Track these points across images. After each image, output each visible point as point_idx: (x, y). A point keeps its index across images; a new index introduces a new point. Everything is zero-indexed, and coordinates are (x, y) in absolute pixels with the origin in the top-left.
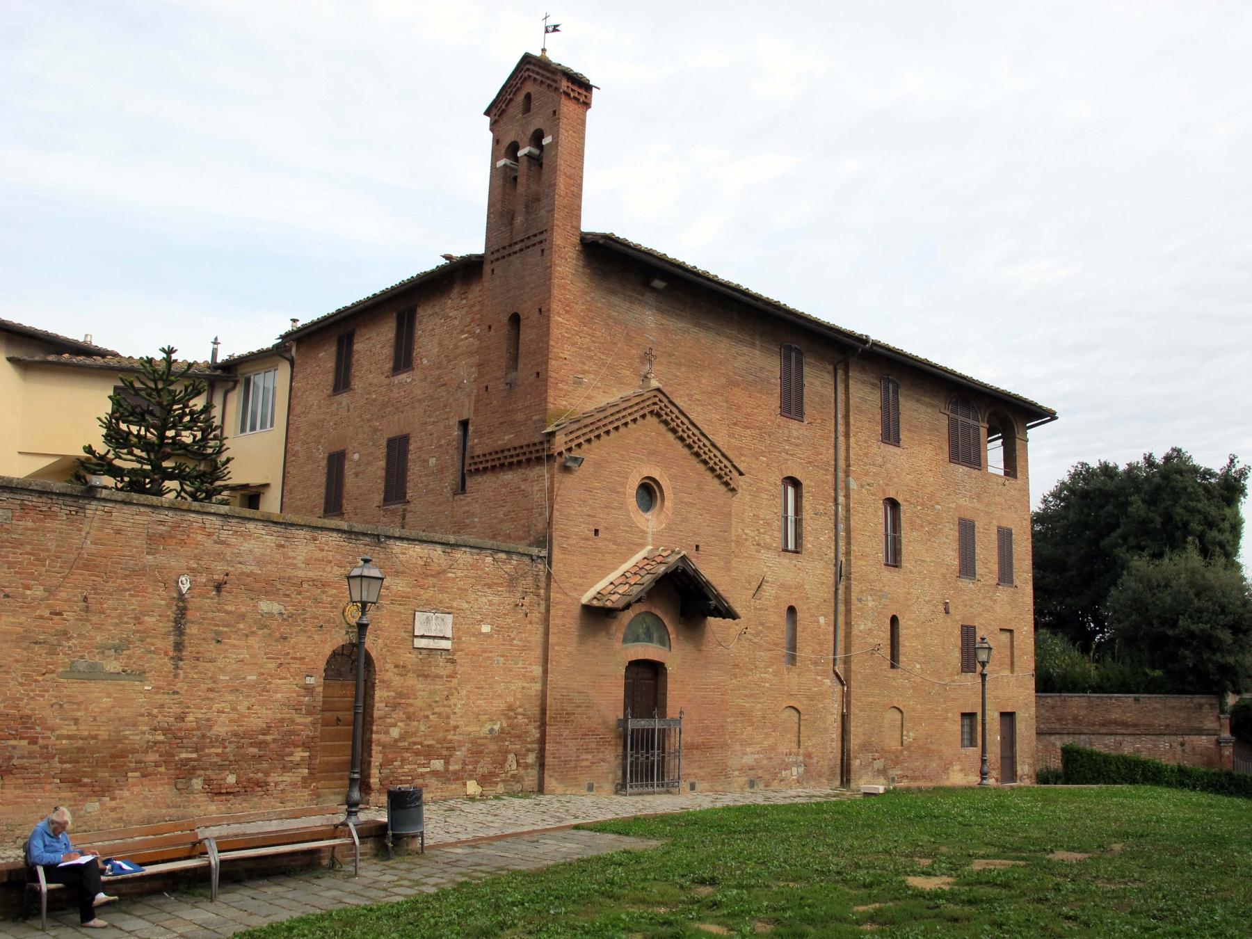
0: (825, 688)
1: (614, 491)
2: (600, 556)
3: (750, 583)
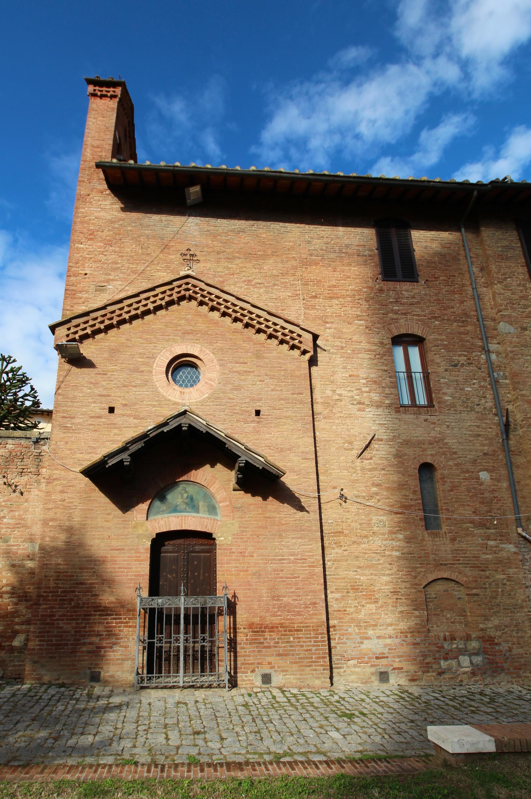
0: (504, 554)
1: (136, 370)
2: (116, 431)
3: (351, 443)
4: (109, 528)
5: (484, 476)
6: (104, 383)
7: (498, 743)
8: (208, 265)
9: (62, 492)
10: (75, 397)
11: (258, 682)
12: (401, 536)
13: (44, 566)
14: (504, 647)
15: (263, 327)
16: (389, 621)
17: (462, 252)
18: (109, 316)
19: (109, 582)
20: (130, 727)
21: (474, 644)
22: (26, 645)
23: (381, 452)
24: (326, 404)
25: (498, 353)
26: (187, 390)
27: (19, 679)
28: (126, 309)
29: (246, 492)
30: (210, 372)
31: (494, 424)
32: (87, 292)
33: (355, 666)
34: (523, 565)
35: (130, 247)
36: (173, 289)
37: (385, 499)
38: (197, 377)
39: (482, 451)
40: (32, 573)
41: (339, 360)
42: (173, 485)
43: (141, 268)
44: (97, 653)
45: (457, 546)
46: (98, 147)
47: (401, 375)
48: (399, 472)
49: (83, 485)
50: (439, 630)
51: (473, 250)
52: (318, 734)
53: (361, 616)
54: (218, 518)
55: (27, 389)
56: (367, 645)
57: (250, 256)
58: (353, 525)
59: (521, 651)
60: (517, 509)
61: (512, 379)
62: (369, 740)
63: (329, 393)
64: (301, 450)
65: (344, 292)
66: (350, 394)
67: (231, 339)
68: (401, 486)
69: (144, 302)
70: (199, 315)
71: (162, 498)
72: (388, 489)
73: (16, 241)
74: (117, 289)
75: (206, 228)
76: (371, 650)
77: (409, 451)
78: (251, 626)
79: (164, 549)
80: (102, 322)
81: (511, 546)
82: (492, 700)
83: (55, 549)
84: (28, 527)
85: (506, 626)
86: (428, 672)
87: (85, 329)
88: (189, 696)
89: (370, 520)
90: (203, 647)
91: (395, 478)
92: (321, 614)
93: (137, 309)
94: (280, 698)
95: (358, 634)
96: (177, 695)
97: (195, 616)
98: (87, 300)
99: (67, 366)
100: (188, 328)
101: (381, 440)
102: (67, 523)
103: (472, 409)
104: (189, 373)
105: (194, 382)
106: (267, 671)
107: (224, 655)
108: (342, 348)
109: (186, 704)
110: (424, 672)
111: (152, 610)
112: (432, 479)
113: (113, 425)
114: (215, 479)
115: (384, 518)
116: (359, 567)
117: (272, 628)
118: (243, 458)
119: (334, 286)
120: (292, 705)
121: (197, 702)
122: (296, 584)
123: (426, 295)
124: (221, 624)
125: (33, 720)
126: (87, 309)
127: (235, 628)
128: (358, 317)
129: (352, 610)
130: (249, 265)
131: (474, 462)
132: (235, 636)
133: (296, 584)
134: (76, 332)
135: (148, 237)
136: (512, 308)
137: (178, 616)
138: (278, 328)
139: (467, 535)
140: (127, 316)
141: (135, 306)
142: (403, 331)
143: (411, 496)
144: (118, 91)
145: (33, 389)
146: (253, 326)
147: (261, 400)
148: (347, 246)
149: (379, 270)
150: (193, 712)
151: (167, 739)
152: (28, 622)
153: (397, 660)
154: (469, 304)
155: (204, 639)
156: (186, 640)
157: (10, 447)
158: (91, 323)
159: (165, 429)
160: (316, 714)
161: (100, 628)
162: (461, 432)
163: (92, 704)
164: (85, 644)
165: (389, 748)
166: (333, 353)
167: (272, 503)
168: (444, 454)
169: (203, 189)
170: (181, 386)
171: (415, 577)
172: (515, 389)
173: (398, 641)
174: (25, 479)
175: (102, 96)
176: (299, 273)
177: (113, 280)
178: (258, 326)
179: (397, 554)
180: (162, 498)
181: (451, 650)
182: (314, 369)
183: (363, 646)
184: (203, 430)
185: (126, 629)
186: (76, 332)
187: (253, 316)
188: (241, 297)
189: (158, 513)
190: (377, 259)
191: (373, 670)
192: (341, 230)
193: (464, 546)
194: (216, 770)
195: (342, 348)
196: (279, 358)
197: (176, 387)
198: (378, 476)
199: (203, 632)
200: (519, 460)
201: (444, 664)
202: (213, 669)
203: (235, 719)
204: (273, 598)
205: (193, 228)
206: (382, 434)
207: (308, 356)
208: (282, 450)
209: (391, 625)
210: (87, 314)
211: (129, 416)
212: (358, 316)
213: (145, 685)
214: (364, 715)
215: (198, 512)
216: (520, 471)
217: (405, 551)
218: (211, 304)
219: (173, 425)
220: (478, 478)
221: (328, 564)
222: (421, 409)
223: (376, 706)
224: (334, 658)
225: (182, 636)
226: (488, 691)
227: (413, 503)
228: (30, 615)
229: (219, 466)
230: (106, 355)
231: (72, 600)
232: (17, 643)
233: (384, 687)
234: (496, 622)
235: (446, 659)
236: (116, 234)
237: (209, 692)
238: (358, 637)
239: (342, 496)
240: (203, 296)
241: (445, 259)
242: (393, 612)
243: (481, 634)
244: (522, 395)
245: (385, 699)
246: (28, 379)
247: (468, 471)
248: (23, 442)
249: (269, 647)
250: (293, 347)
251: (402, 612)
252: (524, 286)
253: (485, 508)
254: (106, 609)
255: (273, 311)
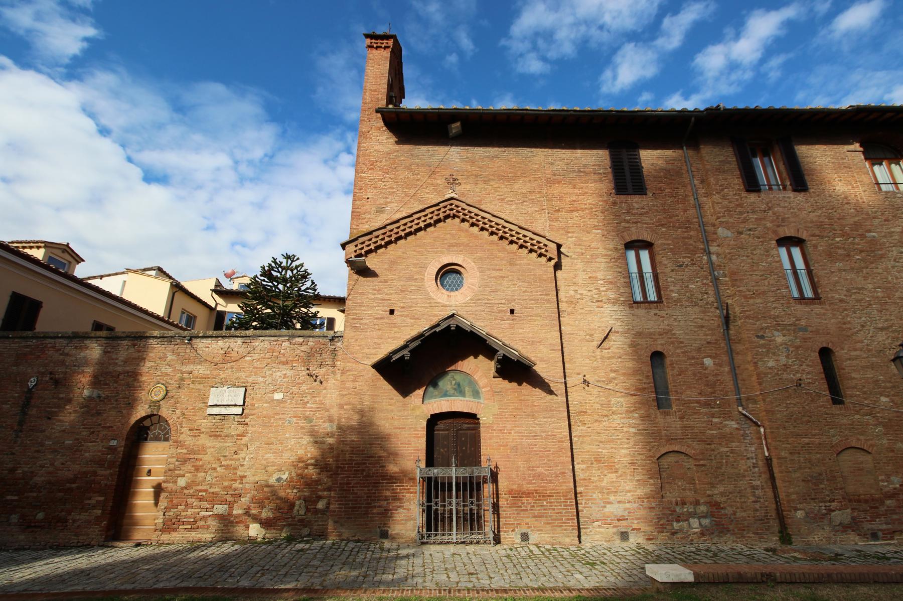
0: (727, 430)
1: (411, 278)
2: (396, 329)
4: (392, 411)
5: (708, 362)
6: (385, 290)
7: (696, 575)
8: (468, 187)
9: (354, 381)
10: (362, 302)
11: (518, 539)
12: (636, 415)
13: (341, 442)
14: (729, 511)
15: (514, 239)
16: (627, 488)
17: (685, 167)
18: (388, 233)
19: (394, 455)
20: (418, 570)
21: (703, 508)
22: (328, 508)
23: (618, 343)
24: (570, 303)
25: (718, 255)
26: (453, 294)
27: (323, 535)
28: (402, 228)
29: (504, 379)
30: (472, 278)
31: (716, 316)
32: (370, 213)
33: (599, 527)
34: (744, 439)
35: (403, 174)
36: (439, 210)
37: (623, 383)
38: (461, 282)
39: (705, 340)
40: (331, 448)
41: (580, 264)
42: (444, 373)
43: (413, 191)
44: (386, 514)
45: (685, 423)
46: (375, 91)
47: (634, 275)
48: (633, 360)
49: (370, 375)
50: (672, 496)
51: (695, 165)
52: (565, 576)
53: (604, 484)
54: (481, 401)
55: (308, 284)
56: (609, 509)
57: (502, 178)
58: (595, 405)
59: (744, 514)
60: (738, 390)
61: (730, 277)
62: (605, 580)
63: (572, 293)
64: (549, 342)
65: (583, 206)
66: (590, 293)
67: (488, 250)
68: (636, 372)
69: (416, 221)
70: (461, 230)
71: (435, 385)
72: (624, 374)
73: (285, 132)
74: (395, 211)
75: (466, 155)
76: (612, 513)
77: (642, 342)
78: (510, 492)
79: (437, 427)
80: (383, 239)
81: (733, 422)
82: (715, 555)
83: (351, 428)
84: (327, 410)
85: (730, 493)
86: (663, 532)
87: (369, 245)
88: (460, 549)
89: (610, 401)
90: (471, 510)
91: (630, 364)
92: (569, 482)
93: (411, 227)
94: (536, 551)
95: (601, 499)
96: (452, 548)
97: (465, 484)
98: (369, 220)
99: (356, 276)
100: (452, 241)
101: (618, 332)
102: (359, 407)
103: (696, 304)
104: (454, 278)
105: (458, 286)
106: (525, 530)
107: (489, 516)
108: (583, 254)
109: (460, 555)
110: (659, 532)
111: (430, 479)
112: (662, 365)
113: (394, 325)
114: (478, 369)
115: (622, 400)
116: (601, 442)
117: (528, 494)
118: (501, 352)
119: (574, 201)
120: (546, 556)
121: (468, 554)
122: (548, 457)
123: (653, 205)
124: (486, 490)
125: (344, 564)
126: (372, 229)
127: (497, 494)
128: (595, 227)
129: (596, 479)
130: (502, 186)
131: (699, 350)
132: (498, 501)
133: (548, 457)
134: (362, 248)
135: (418, 165)
136: (729, 215)
137: (450, 484)
138: (527, 239)
139: (695, 413)
140: (403, 234)
141: (409, 224)
142: (634, 238)
143: (645, 381)
144: (391, 42)
145: (313, 283)
146: (507, 239)
147: (514, 300)
148: (585, 166)
149: (613, 185)
150: (466, 560)
151: (448, 577)
152: (329, 489)
153: (636, 522)
154: (692, 212)
155: (472, 503)
156: (457, 504)
157: (311, 344)
158: (374, 240)
159: (438, 329)
160: (564, 562)
161: (388, 493)
162: (687, 324)
163: (385, 554)
164: (375, 507)
165: (620, 585)
166: (574, 259)
167: (526, 388)
168: (672, 343)
169: (462, 125)
170: (448, 290)
171: (650, 450)
172: (733, 286)
173: (636, 505)
174: (323, 370)
175: (377, 48)
176: (544, 191)
177: (390, 202)
178: (510, 238)
179: (634, 430)
180: (435, 385)
181: (682, 514)
182: (559, 272)
183: (606, 510)
184: (468, 329)
185: (408, 495)
186: (362, 248)
187: (507, 230)
188: (496, 214)
189: (431, 397)
190: (610, 176)
191: (615, 530)
192: (579, 152)
193: (691, 423)
194: (488, 593)
195: (583, 254)
196: (529, 264)
197: (444, 291)
198: (616, 364)
199: (471, 497)
200: (739, 347)
201: (676, 525)
202: (480, 527)
203: (500, 565)
204: (529, 468)
205: (454, 156)
206: (618, 327)
207: (553, 262)
208: (533, 343)
209: (629, 491)
210: (371, 233)
211: (407, 316)
212: (595, 226)
213: (425, 541)
214: (604, 564)
215: (464, 396)
216: (740, 357)
217: (641, 427)
218: (471, 221)
219: (444, 326)
220: (703, 364)
221: (575, 439)
222: (652, 305)
223: (615, 558)
224: (581, 520)
225: (454, 500)
226: (714, 548)
227: (646, 386)
228: (330, 484)
229: (481, 357)
230: (386, 266)
231: (363, 470)
232: (321, 505)
233: (625, 545)
234: (722, 489)
235: (678, 521)
236: (392, 164)
237: (478, 547)
238: (601, 502)
239: (585, 381)
240: (464, 214)
241: (670, 174)
242: (631, 480)
243: (707, 499)
244: (740, 291)
245: (624, 553)
246: (309, 274)
247: (693, 358)
248: (321, 339)
249: (526, 510)
250: (540, 255)
251: (639, 480)
252: (739, 195)
253: (709, 390)
254: (392, 478)
255: (523, 226)
